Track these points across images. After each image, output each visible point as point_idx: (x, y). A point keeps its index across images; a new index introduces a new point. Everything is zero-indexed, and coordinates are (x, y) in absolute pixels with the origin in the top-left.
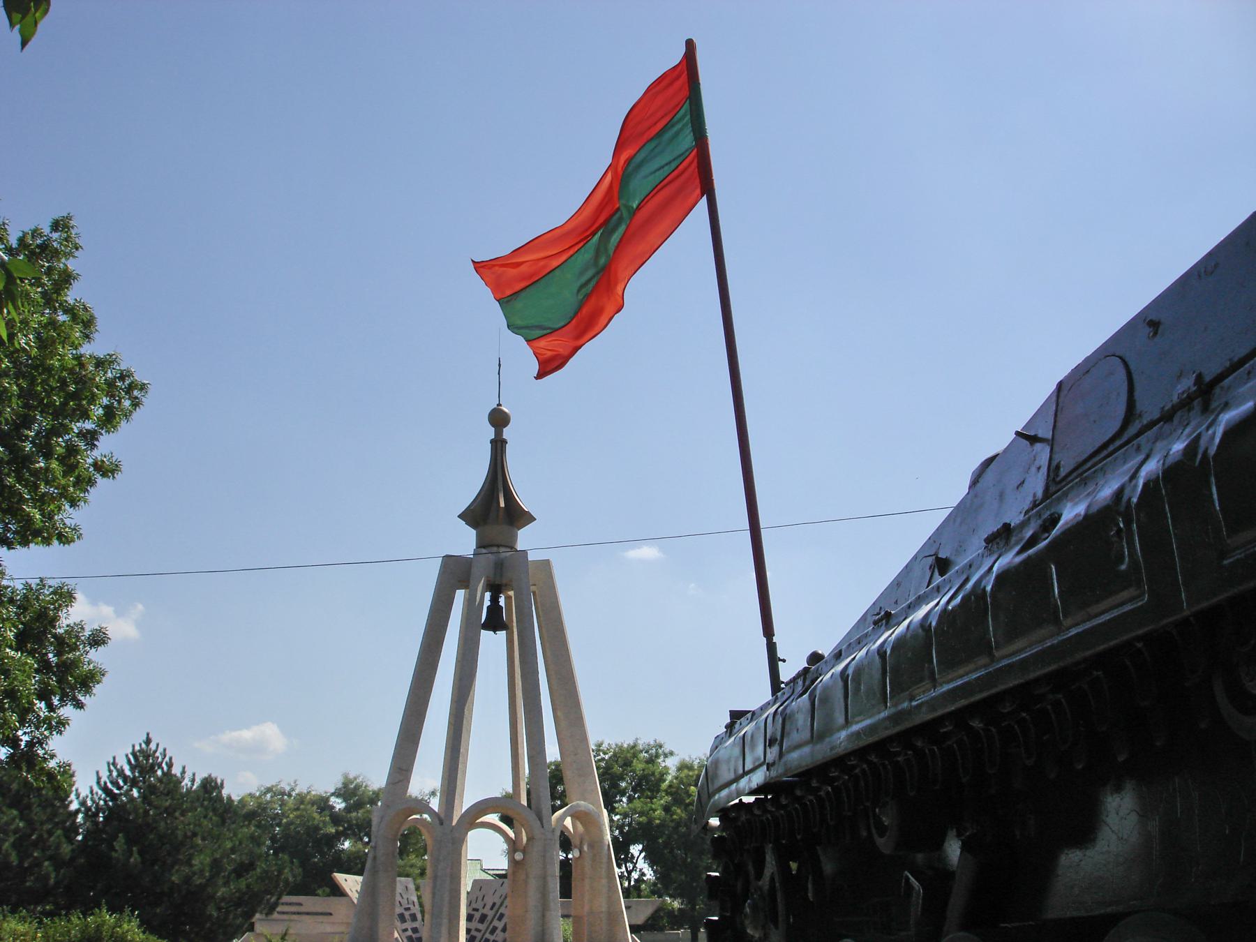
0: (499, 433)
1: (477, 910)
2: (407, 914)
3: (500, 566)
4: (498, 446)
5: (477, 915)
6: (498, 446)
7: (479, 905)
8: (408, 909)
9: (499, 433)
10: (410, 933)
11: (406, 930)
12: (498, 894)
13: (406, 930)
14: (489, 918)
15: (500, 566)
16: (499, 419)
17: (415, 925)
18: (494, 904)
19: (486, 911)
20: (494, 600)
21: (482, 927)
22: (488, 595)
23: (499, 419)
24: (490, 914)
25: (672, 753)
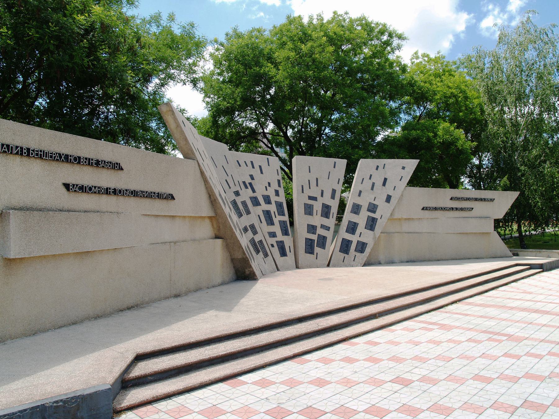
1: (315, 199)
5: (317, 207)
7: (314, 192)
17: (246, 221)
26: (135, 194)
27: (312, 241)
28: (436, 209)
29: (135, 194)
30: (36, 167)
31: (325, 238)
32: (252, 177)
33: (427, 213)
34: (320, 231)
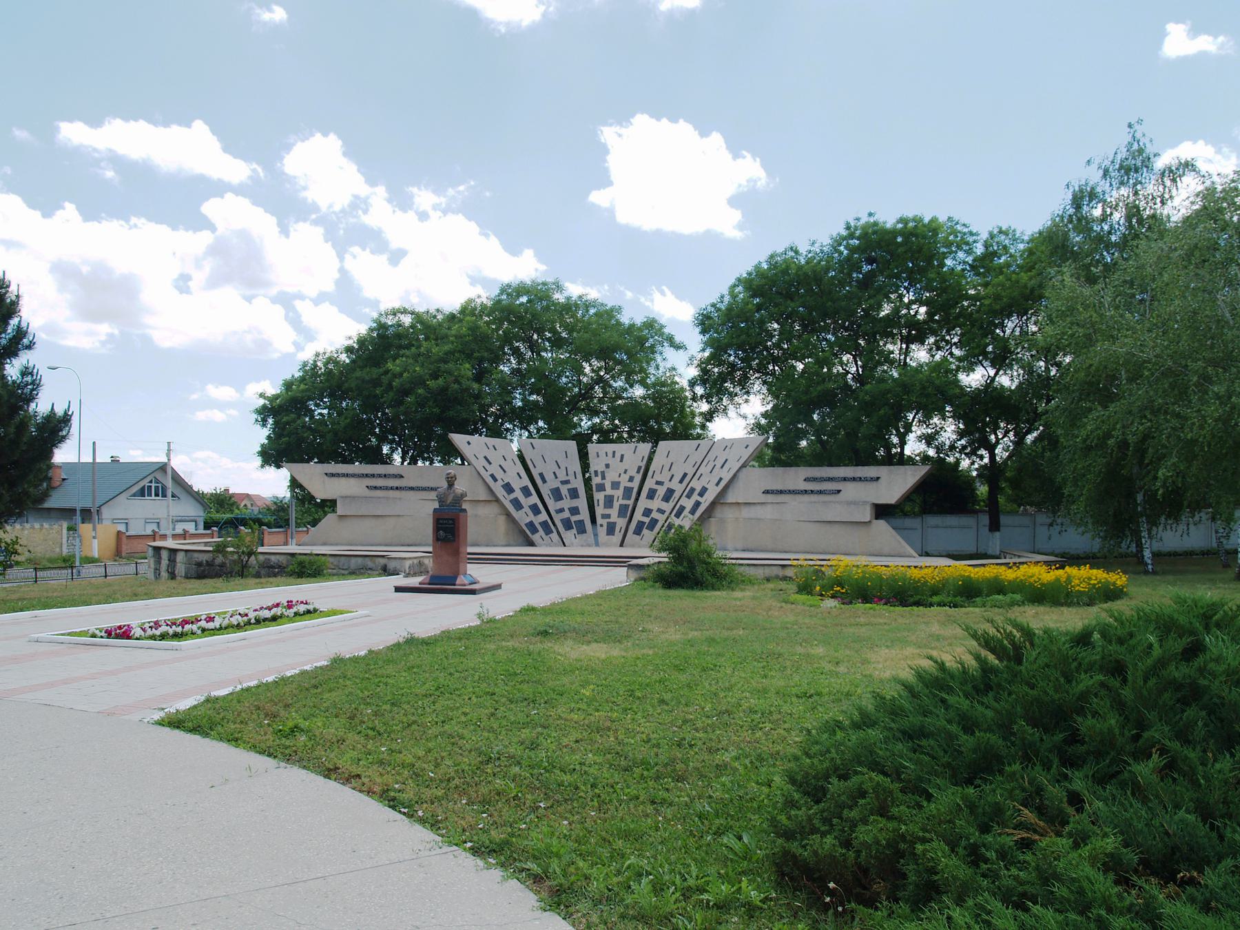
2: (564, 490)
5: (661, 491)
7: (664, 477)
8: (567, 482)
10: (566, 514)
11: (561, 510)
12: (691, 461)
13: (561, 510)
14: (677, 495)
17: (575, 503)
18: (685, 475)
19: (675, 485)
21: (667, 507)
24: (679, 488)
26: (412, 489)
27: (643, 523)
28: (781, 492)
29: (412, 489)
30: (352, 481)
31: (656, 521)
32: (607, 466)
33: (770, 498)
34: (655, 515)
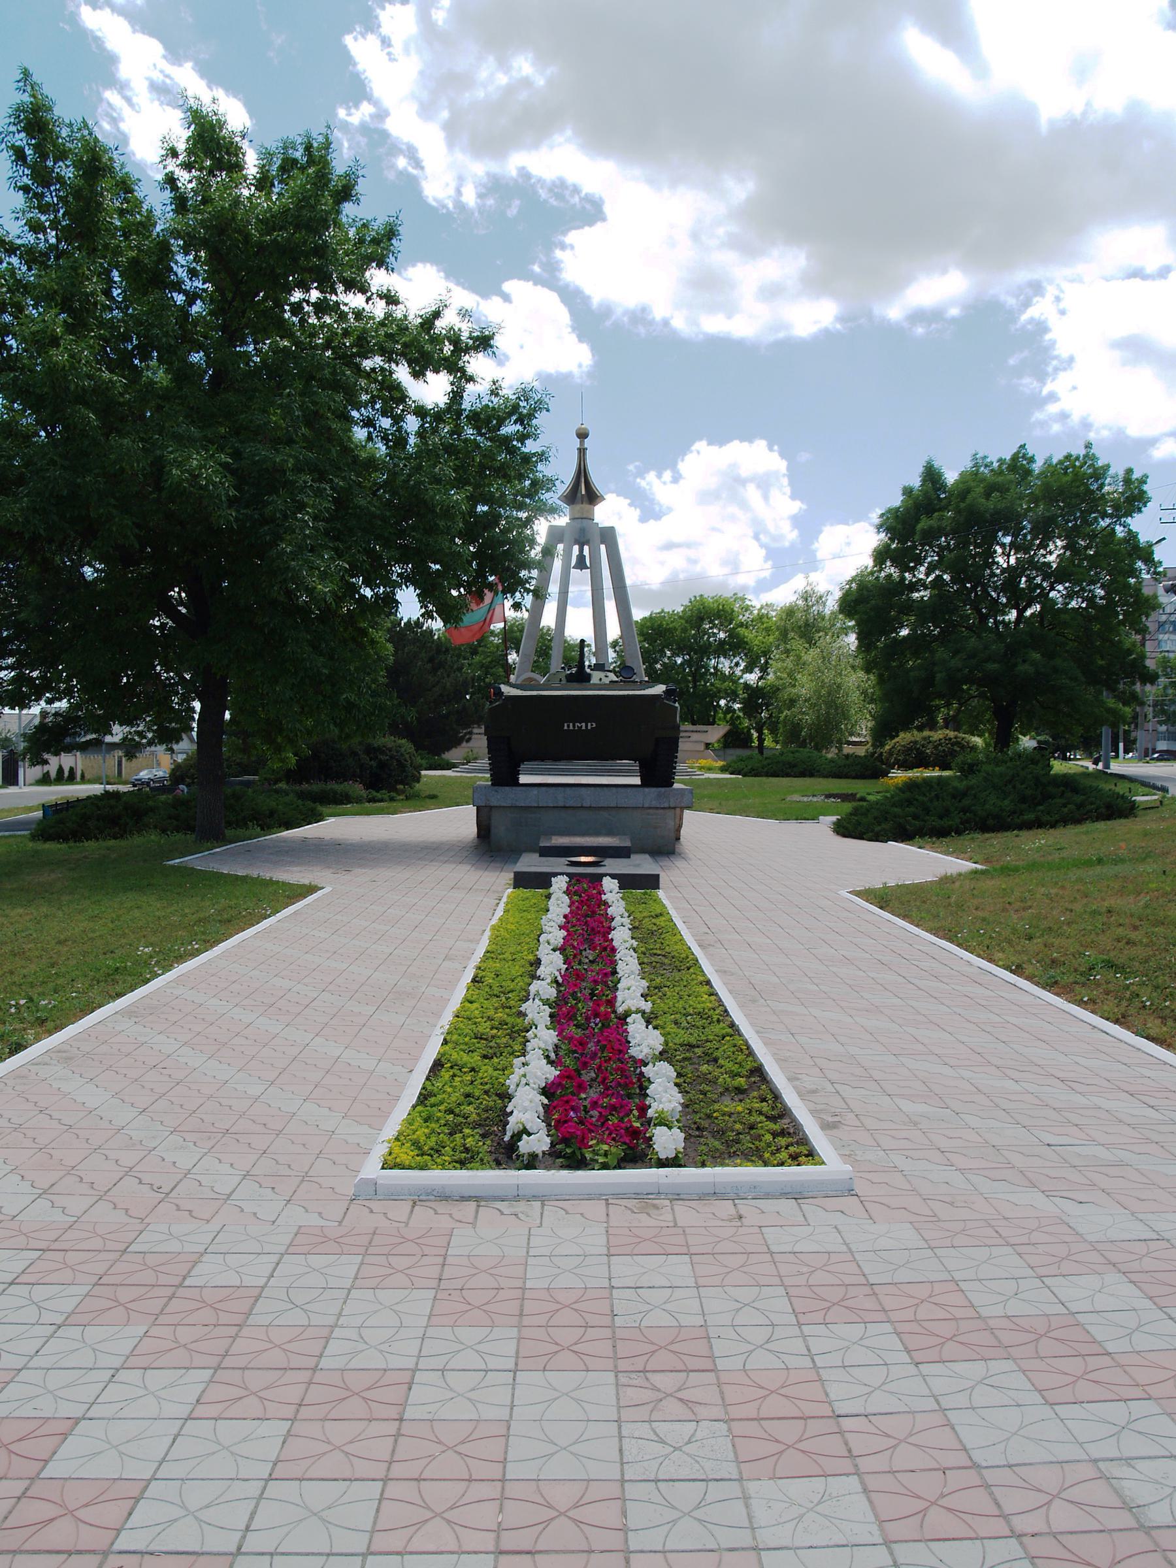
0: (582, 443)
3: (583, 531)
4: (582, 452)
6: (582, 452)
9: (582, 443)
15: (583, 531)
16: (582, 435)
20: (581, 550)
22: (576, 548)
23: (582, 435)
25: (410, 280)
